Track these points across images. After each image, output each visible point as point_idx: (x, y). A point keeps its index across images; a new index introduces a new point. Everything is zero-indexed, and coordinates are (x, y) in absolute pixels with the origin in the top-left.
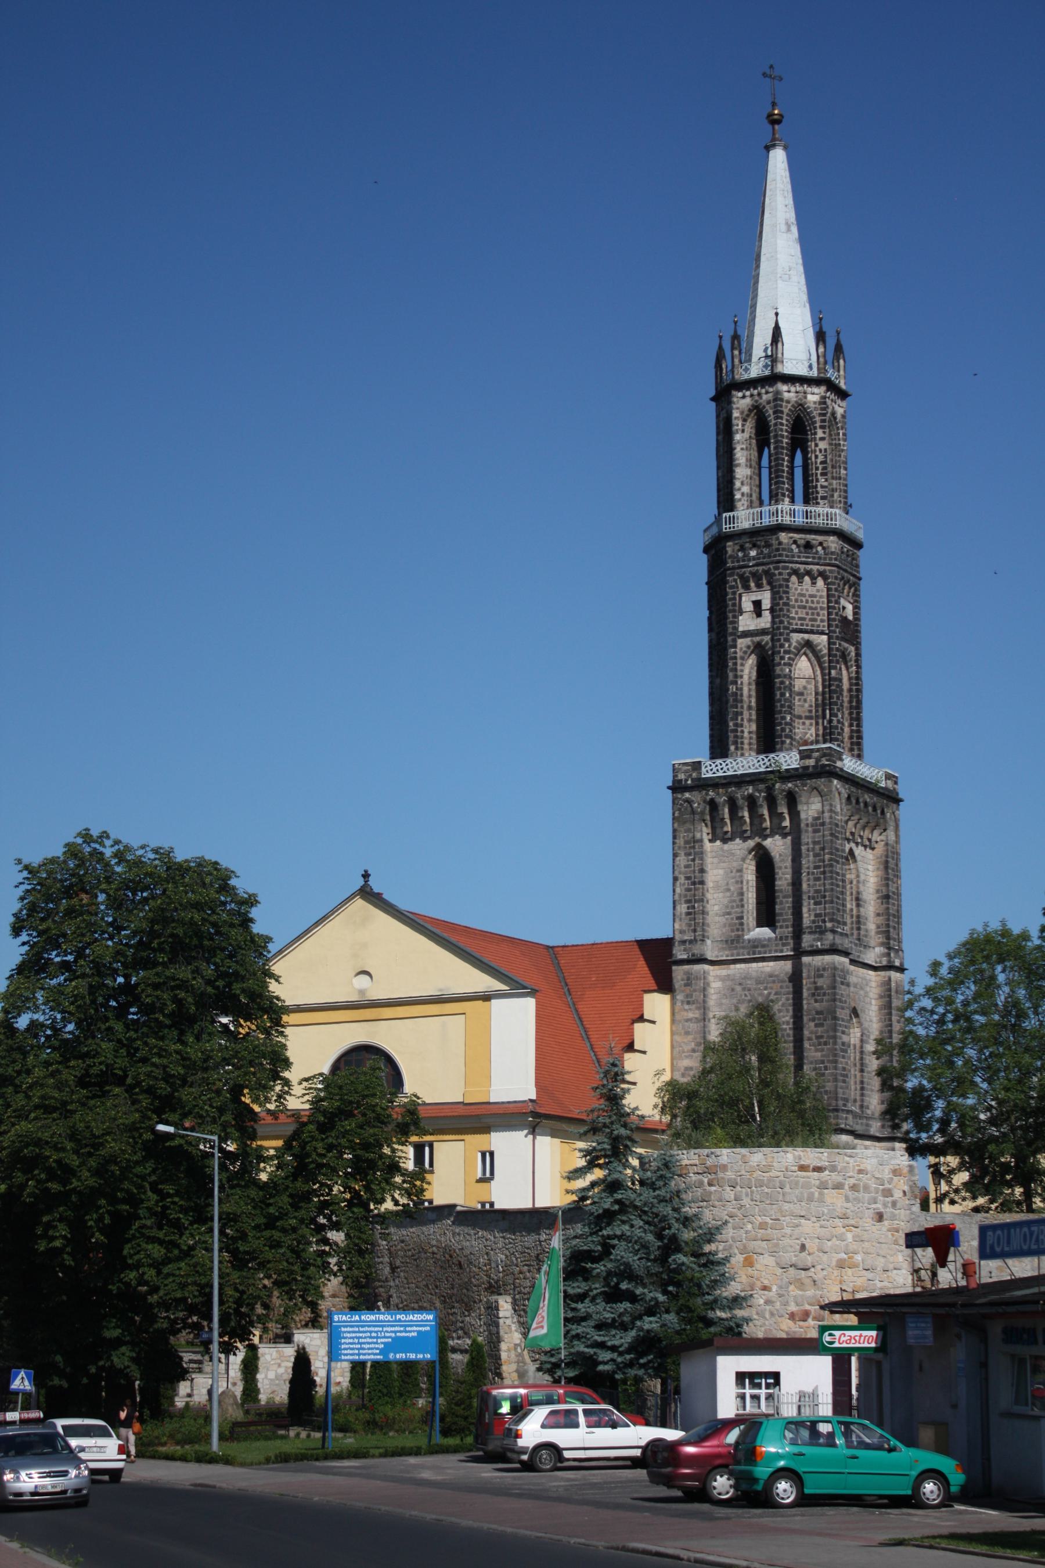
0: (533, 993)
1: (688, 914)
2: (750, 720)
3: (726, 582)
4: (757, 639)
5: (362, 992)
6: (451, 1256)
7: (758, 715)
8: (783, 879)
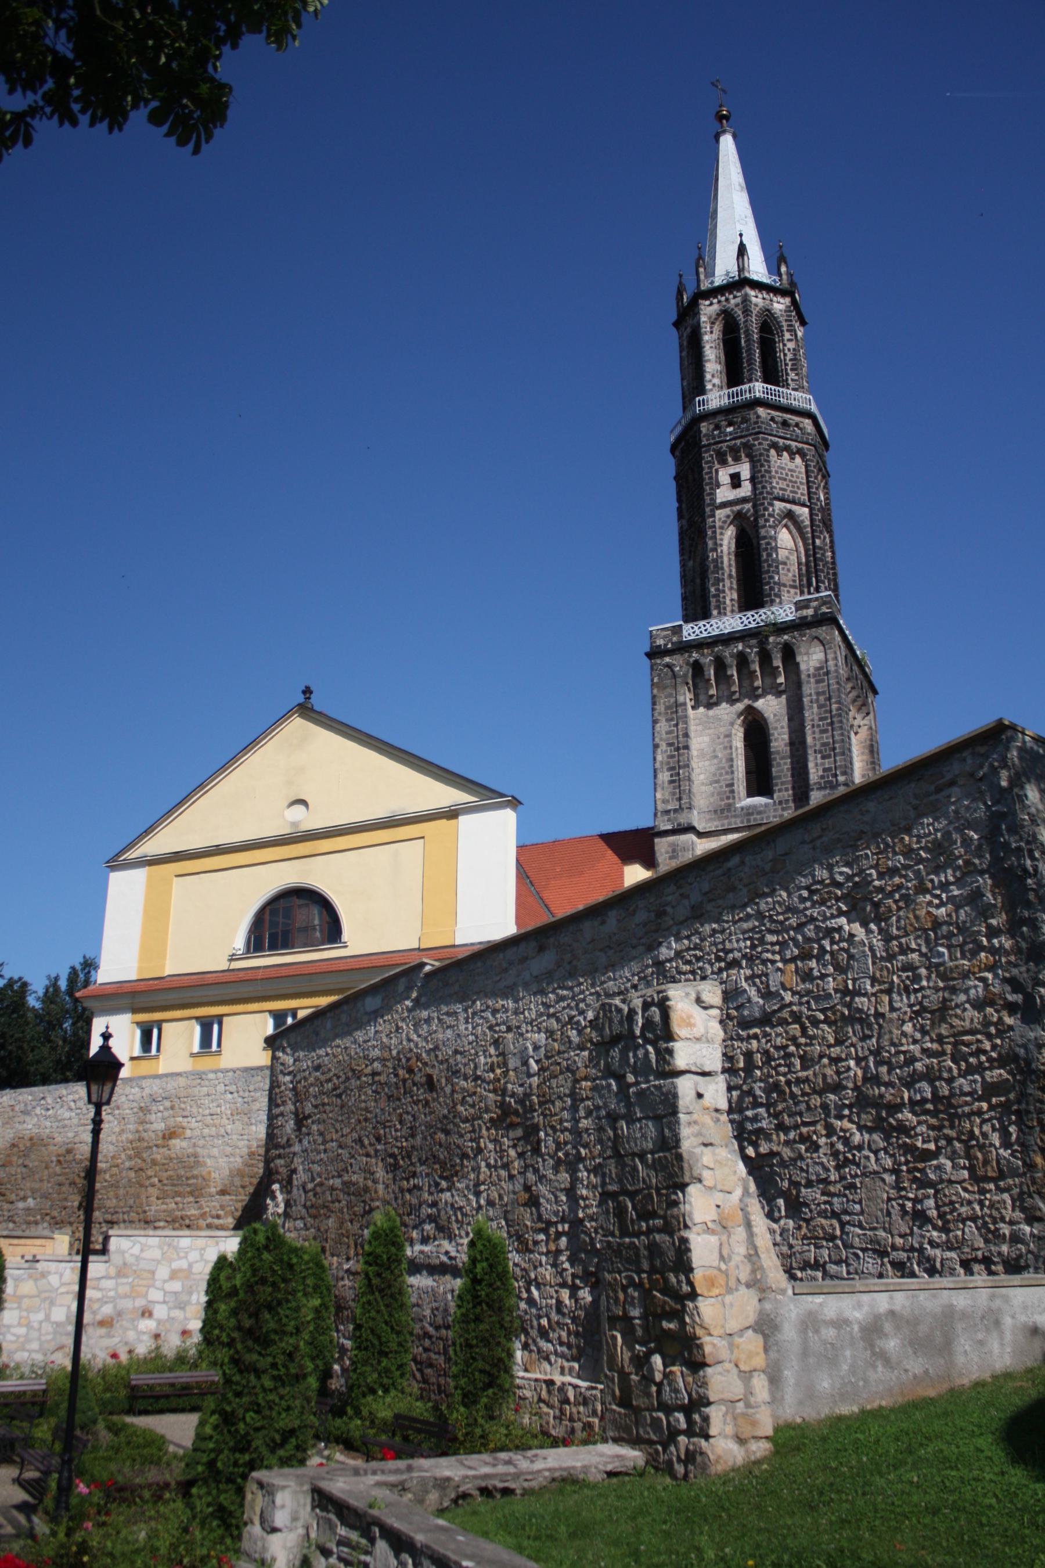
0: (514, 803)
1: (671, 782)
2: (731, 588)
3: (702, 458)
4: (738, 508)
5: (294, 824)
6: (410, 1071)
7: (738, 584)
8: (780, 739)
